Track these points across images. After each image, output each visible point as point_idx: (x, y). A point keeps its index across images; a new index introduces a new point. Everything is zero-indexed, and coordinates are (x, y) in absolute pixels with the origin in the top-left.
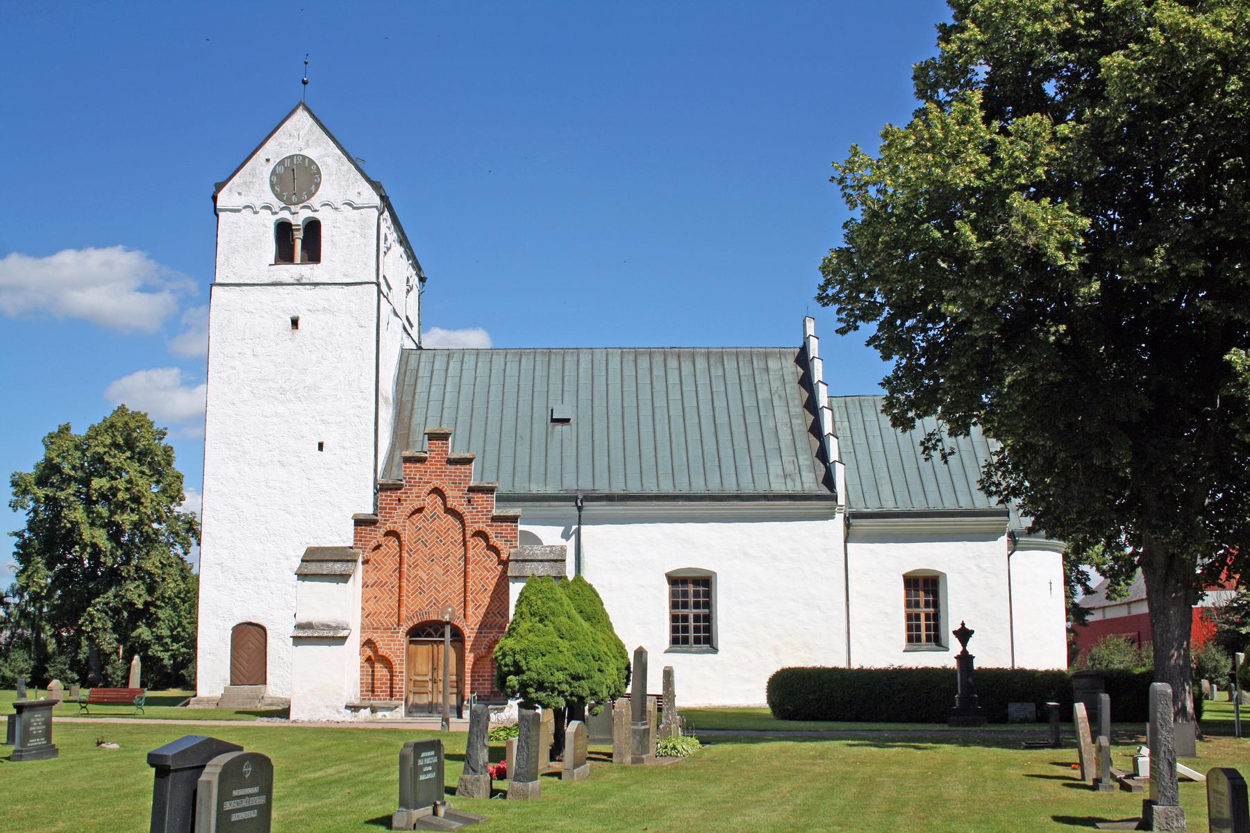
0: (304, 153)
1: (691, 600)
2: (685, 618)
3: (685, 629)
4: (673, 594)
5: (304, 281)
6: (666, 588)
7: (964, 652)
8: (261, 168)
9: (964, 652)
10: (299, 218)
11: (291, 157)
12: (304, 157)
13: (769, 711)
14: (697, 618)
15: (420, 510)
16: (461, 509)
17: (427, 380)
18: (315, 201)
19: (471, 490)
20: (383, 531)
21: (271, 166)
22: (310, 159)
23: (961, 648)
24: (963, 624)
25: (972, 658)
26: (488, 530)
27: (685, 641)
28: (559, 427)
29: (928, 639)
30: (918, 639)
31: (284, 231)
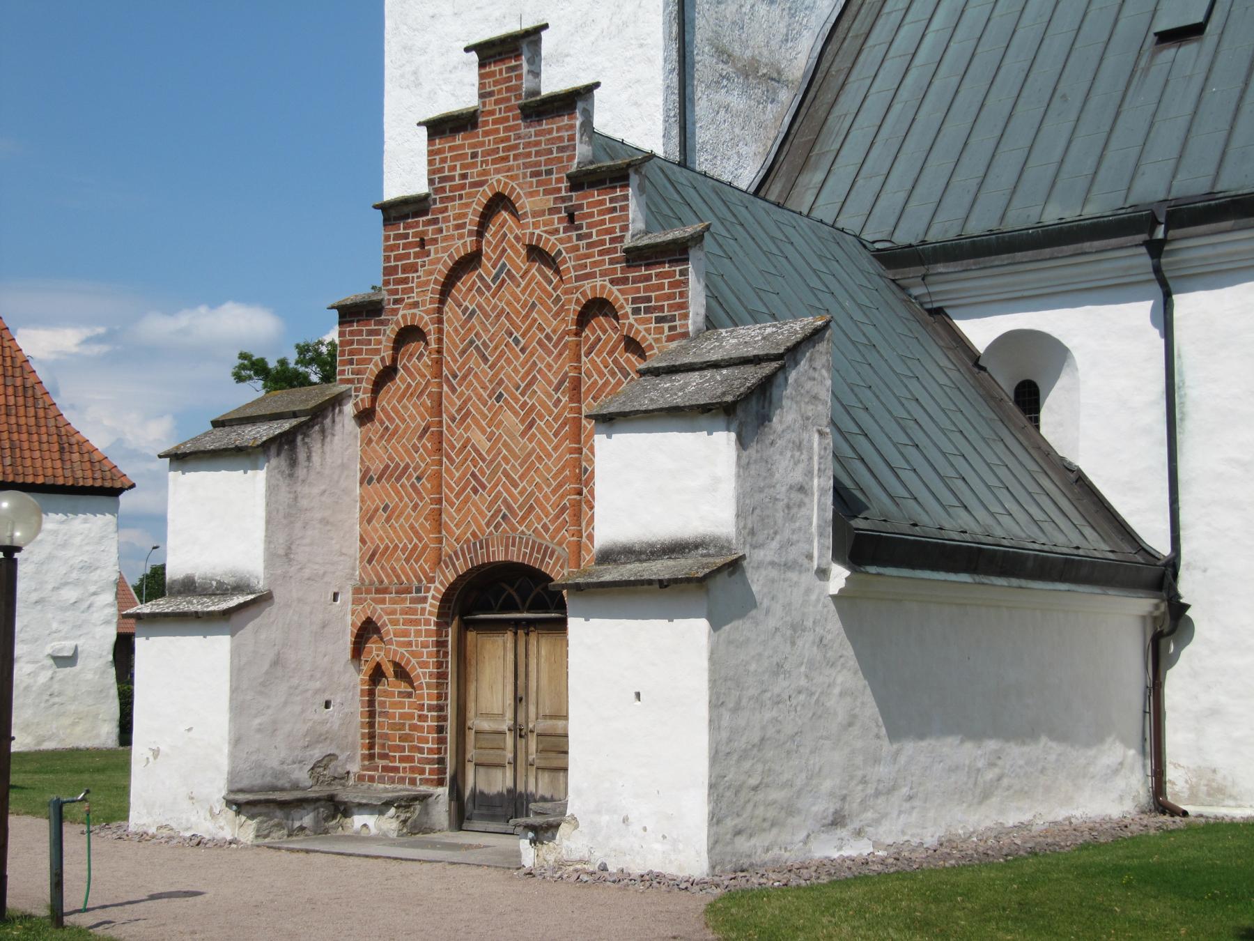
15: (469, 262)
16: (551, 244)
20: (391, 331)
28: (1169, 53)
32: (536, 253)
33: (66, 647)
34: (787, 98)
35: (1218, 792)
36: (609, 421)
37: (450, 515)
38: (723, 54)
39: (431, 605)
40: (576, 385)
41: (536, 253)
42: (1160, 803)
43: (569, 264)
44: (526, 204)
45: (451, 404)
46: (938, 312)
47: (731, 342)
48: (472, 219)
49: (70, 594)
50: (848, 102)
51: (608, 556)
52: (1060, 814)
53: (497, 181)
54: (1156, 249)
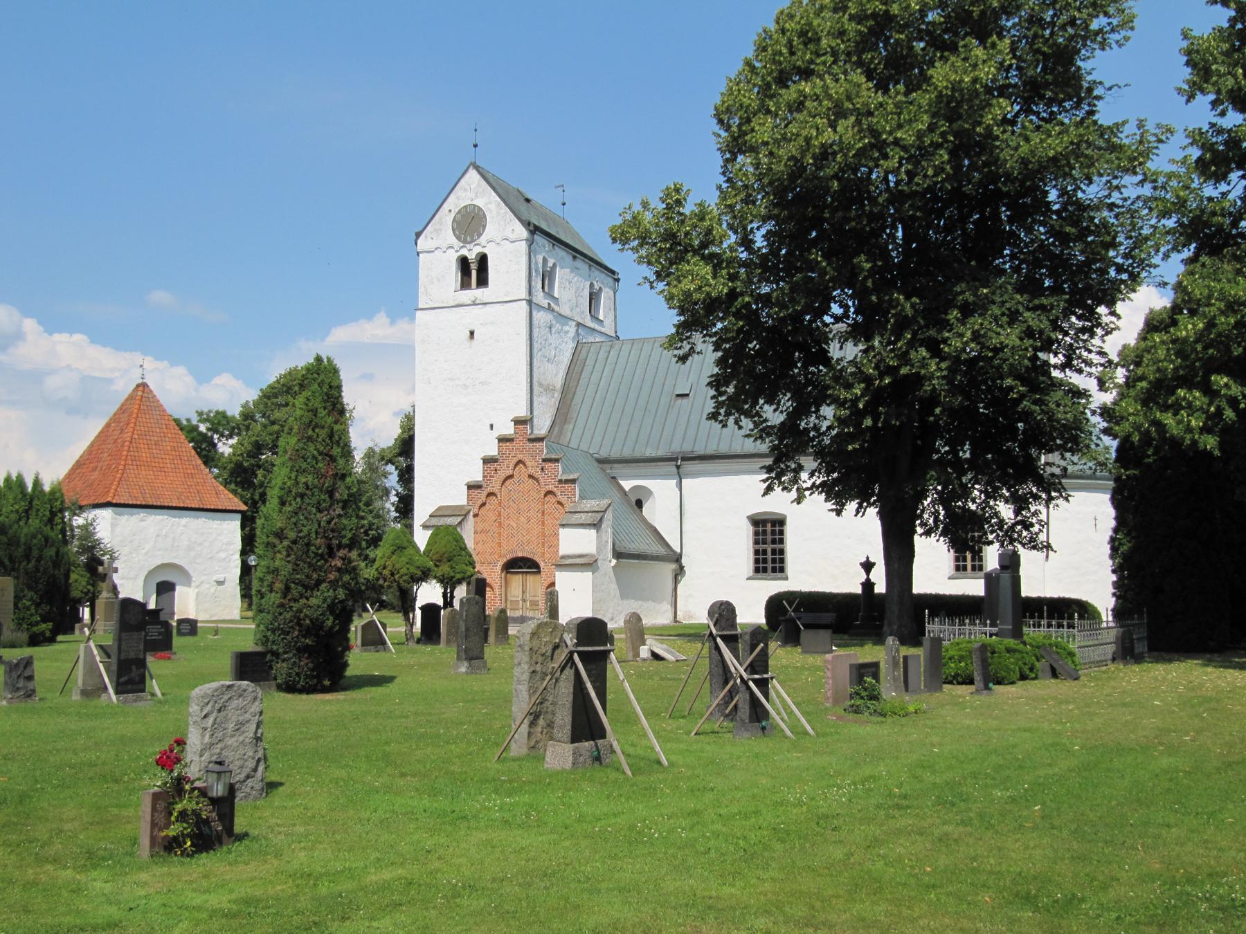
0: (473, 203)
1: (769, 538)
2: (765, 552)
3: (765, 561)
4: (756, 533)
5: (478, 302)
6: (747, 531)
7: (868, 580)
8: (446, 218)
9: (868, 580)
10: (472, 256)
11: (466, 207)
12: (475, 206)
13: (766, 628)
14: (774, 552)
15: (511, 476)
16: (536, 475)
17: (591, 367)
18: (483, 239)
19: (544, 460)
20: (485, 493)
21: (452, 215)
22: (479, 207)
23: (865, 577)
24: (868, 558)
25: (873, 584)
26: (555, 490)
27: (765, 570)
28: (680, 401)
29: (974, 568)
30: (965, 568)
31: (464, 263)
32: (531, 476)
33: (220, 577)
34: (557, 395)
35: (691, 617)
36: (563, 526)
37: (504, 543)
38: (540, 385)
39: (499, 567)
40: (543, 512)
41: (531, 476)
42: (676, 621)
43: (542, 480)
44: (528, 464)
45: (504, 514)
46: (614, 478)
47: (590, 504)
48: (512, 466)
49: (222, 555)
50: (578, 399)
51: (563, 557)
52: (653, 622)
53: (520, 457)
54: (678, 467)
